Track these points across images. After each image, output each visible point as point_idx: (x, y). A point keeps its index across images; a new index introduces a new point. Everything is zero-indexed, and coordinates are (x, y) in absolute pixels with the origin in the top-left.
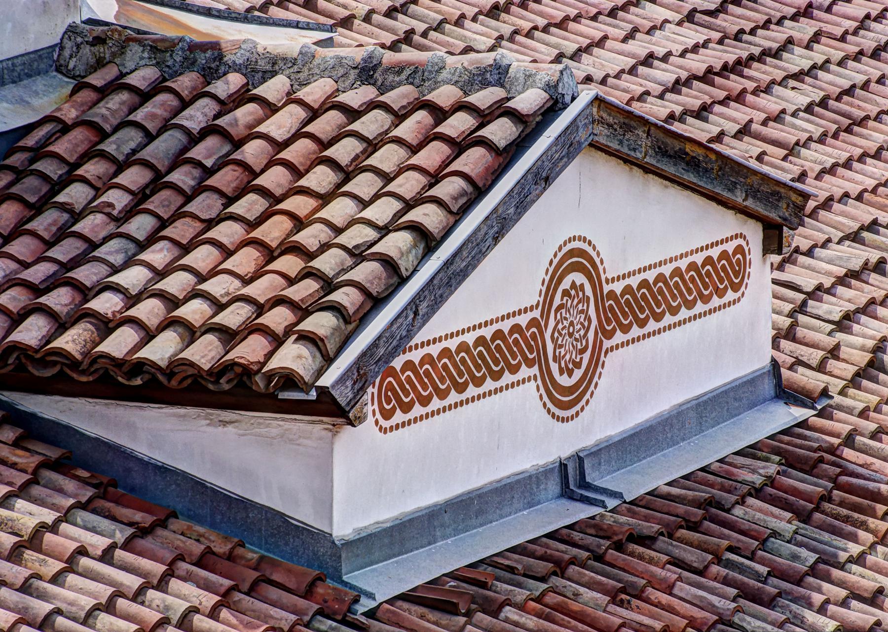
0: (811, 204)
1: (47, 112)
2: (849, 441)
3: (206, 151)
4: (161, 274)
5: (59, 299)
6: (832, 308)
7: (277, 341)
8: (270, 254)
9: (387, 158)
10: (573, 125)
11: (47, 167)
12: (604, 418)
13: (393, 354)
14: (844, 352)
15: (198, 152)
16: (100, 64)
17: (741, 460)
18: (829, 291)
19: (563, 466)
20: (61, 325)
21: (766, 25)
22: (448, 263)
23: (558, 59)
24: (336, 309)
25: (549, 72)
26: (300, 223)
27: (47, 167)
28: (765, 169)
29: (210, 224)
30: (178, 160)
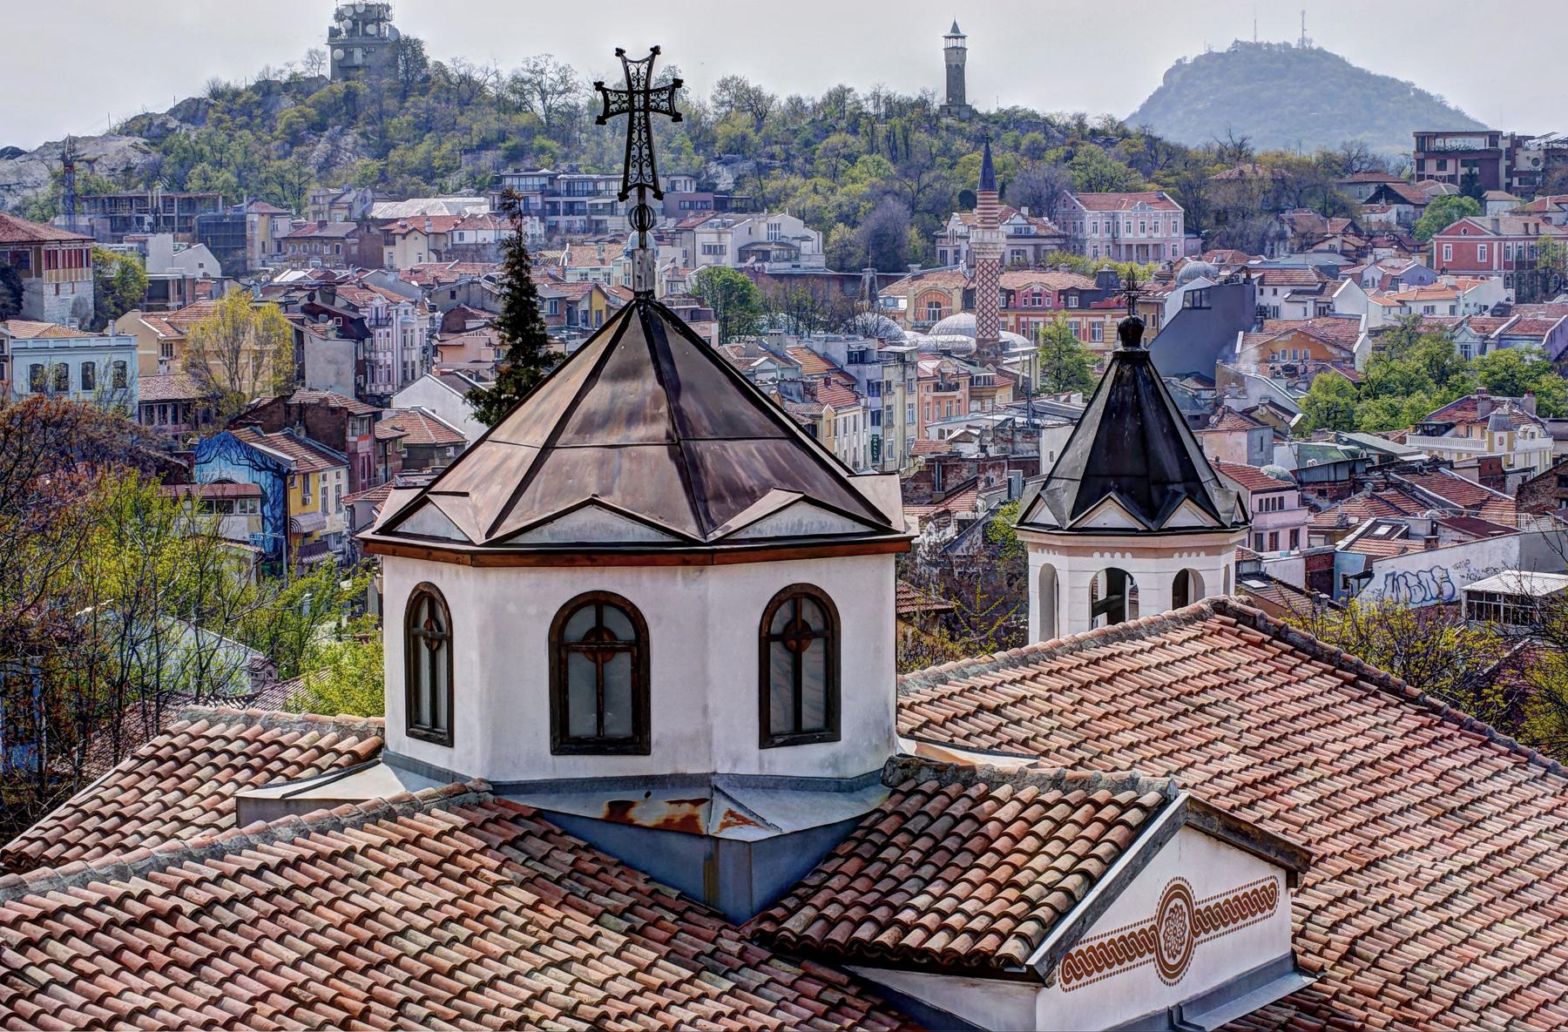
0: (1314, 859)
1: (876, 806)
2: (1336, 996)
3: (964, 828)
4: (938, 899)
5: (881, 913)
6: (1326, 919)
7: (1003, 938)
8: (1000, 887)
9: (1067, 831)
10: (1176, 813)
11: (874, 837)
12: (1193, 984)
13: (1071, 945)
14: (1333, 944)
15: (959, 829)
16: (906, 779)
17: (1273, 1008)
18: (1325, 909)
19: (1170, 1011)
20: (882, 928)
21: (1287, 755)
22: (1103, 893)
23: (1167, 774)
24: (1037, 919)
25: (1162, 782)
26: (1017, 869)
27: (874, 837)
28: (1288, 838)
29: (966, 870)
30: (948, 834)
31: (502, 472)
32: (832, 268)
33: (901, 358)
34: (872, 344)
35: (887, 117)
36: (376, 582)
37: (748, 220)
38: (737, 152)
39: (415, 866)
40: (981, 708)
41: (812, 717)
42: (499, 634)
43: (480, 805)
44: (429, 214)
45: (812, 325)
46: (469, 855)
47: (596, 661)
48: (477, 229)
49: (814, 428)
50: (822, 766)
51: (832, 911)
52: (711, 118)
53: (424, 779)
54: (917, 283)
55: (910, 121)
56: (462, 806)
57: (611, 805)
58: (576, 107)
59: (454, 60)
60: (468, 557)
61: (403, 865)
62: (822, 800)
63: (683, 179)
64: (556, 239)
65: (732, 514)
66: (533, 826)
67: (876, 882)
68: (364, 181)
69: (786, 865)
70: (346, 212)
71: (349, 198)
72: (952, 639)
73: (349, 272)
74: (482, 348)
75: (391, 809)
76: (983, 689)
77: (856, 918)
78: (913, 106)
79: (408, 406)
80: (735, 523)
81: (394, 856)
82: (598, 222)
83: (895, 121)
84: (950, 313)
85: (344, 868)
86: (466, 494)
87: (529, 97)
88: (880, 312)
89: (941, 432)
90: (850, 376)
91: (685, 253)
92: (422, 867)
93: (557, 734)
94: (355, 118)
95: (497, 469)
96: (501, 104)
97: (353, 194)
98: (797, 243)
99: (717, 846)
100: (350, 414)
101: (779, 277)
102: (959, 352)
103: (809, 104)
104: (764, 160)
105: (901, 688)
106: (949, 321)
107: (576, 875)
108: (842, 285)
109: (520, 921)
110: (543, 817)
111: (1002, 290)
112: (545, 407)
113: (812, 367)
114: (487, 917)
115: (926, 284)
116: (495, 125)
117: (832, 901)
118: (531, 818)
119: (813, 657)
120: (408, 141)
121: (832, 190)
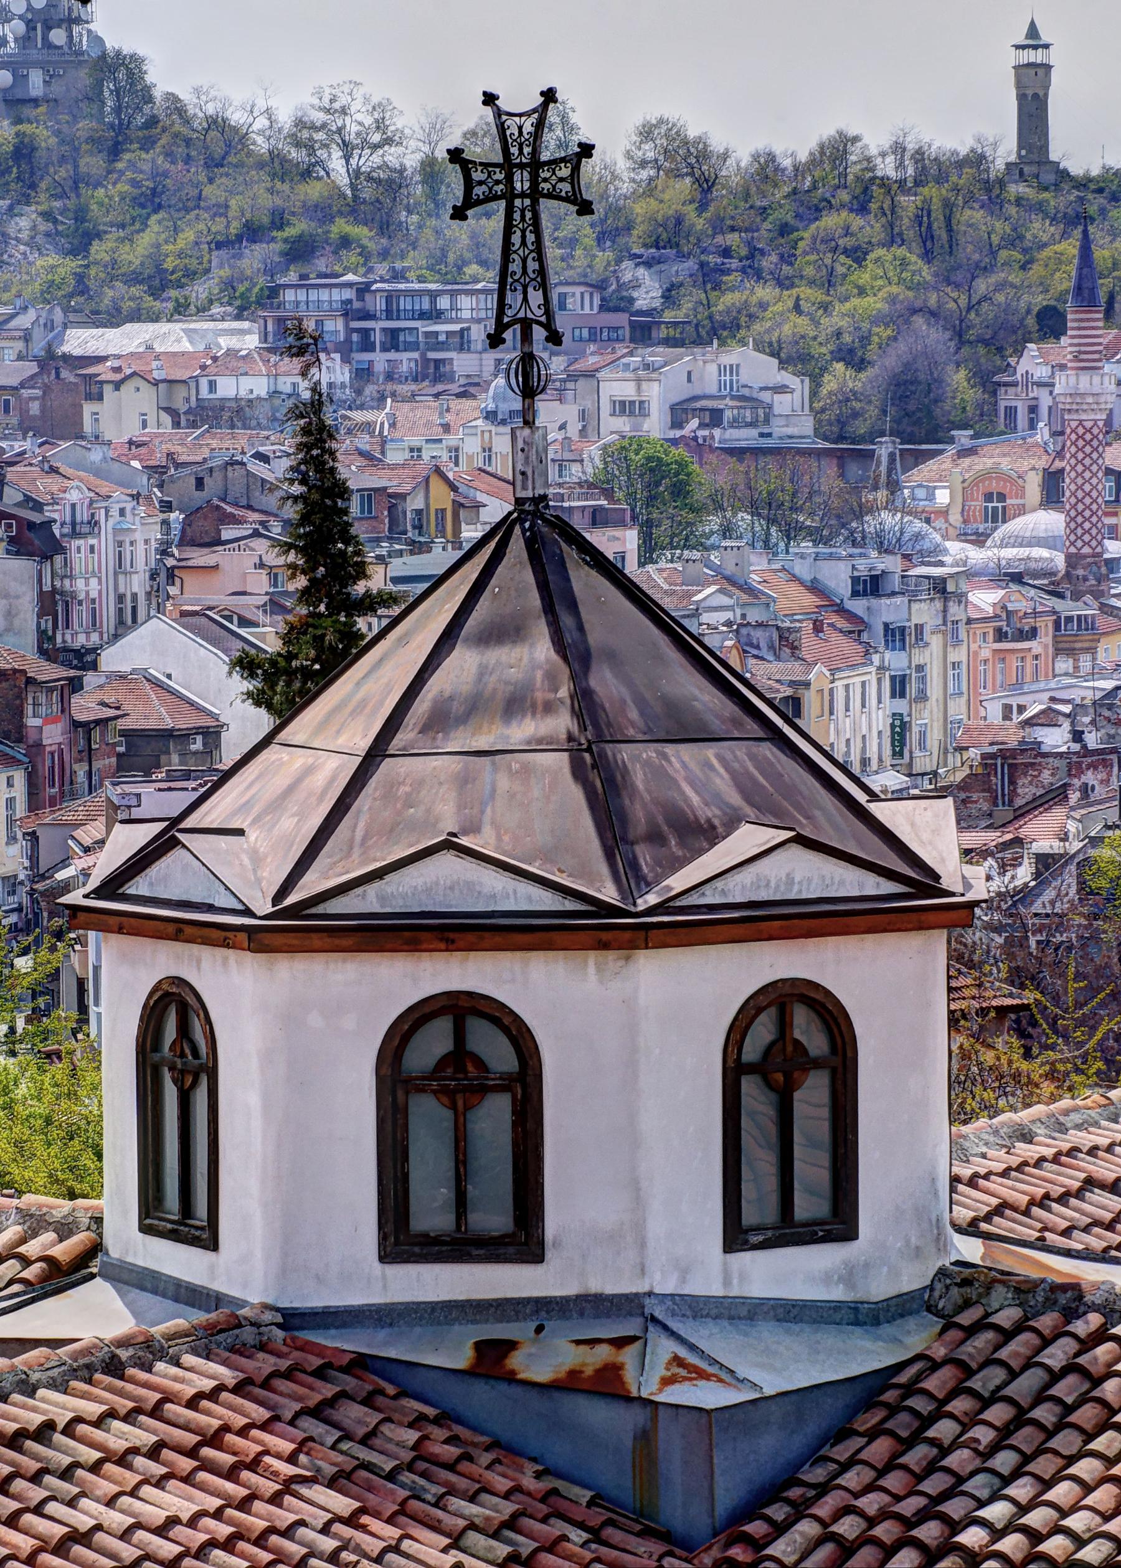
1: (918, 1350)
3: (1067, 1389)
11: (918, 1403)
15: (1058, 1390)
16: (967, 1304)
27: (918, 1403)
29: (1071, 1460)
30: (1040, 1398)
31: (299, 795)
32: (826, 438)
33: (939, 587)
34: (891, 564)
35: (917, 183)
36: (75, 959)
37: (686, 359)
38: (669, 244)
39: (154, 1453)
40: (1090, 1182)
41: (808, 1205)
42: (297, 1073)
43: (263, 1347)
44: (159, 348)
45: (791, 532)
46: (243, 1432)
47: (453, 1107)
48: (239, 374)
49: (796, 703)
50: (827, 1279)
51: (848, 1527)
52: (626, 188)
53: (169, 1304)
54: (967, 462)
55: (957, 189)
56: (232, 1349)
57: (479, 1346)
58: (402, 171)
59: (197, 91)
60: (243, 937)
61: (135, 1451)
62: (829, 1338)
63: (578, 290)
64: (370, 390)
65: (676, 864)
66: (350, 1383)
67: (920, 1478)
68: (48, 294)
69: (769, 1449)
70: (20, 345)
71: (25, 321)
72: (1027, 1055)
73: (27, 444)
74: (251, 571)
75: (114, 1356)
76: (1093, 1151)
77: (887, 1539)
78: (961, 163)
79: (125, 668)
80: (678, 882)
81: (121, 1436)
82: (438, 363)
83: (932, 192)
84: (1022, 511)
85: (36, 1457)
86: (240, 832)
87: (322, 153)
88: (906, 511)
89: (1007, 708)
90: (857, 614)
91: (583, 415)
92: (166, 1454)
93: (390, 1227)
94: (33, 186)
95: (290, 790)
96: (277, 166)
97: (31, 314)
98: (766, 396)
99: (654, 1419)
100: (30, 681)
101: (738, 452)
102: (1036, 575)
103: (787, 163)
104: (713, 259)
105: (958, 1150)
106: (1015, 526)
107: (422, 1465)
108: (841, 466)
109: (328, 1544)
110: (366, 1368)
111: (1109, 471)
112: (371, 687)
113: (792, 602)
114: (274, 1539)
115: (982, 463)
116: (267, 201)
117: (847, 1510)
118: (346, 1370)
119: (812, 1098)
120: (123, 226)
121: (825, 307)
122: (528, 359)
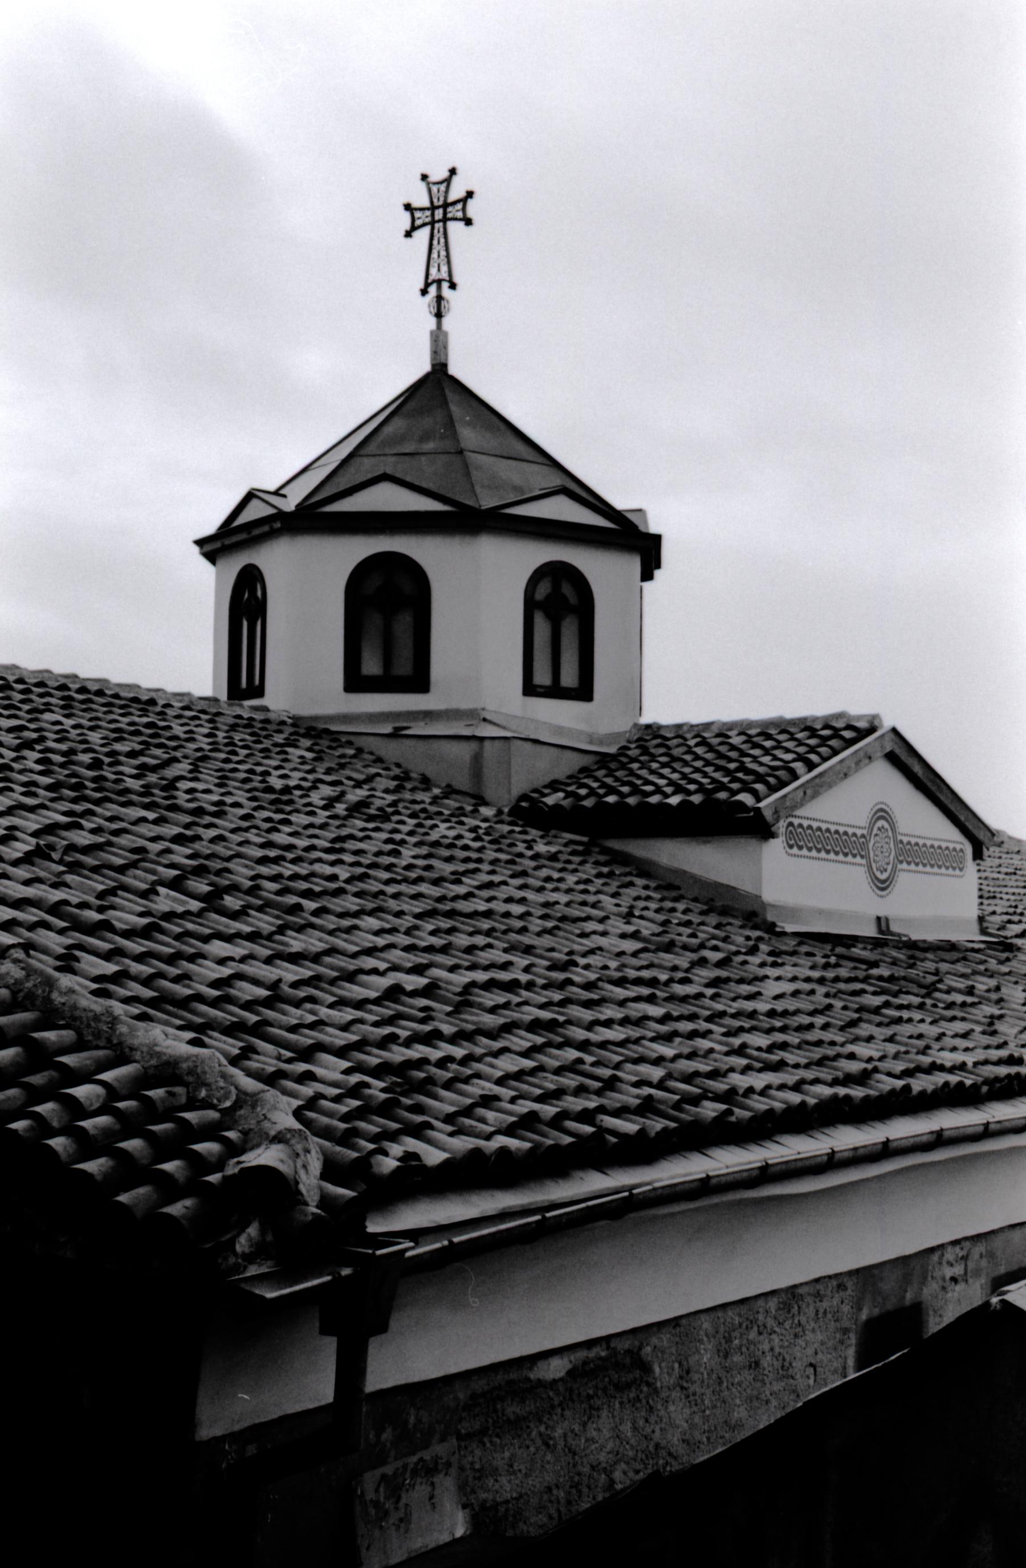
99: (481, 748)
122: (439, 298)
